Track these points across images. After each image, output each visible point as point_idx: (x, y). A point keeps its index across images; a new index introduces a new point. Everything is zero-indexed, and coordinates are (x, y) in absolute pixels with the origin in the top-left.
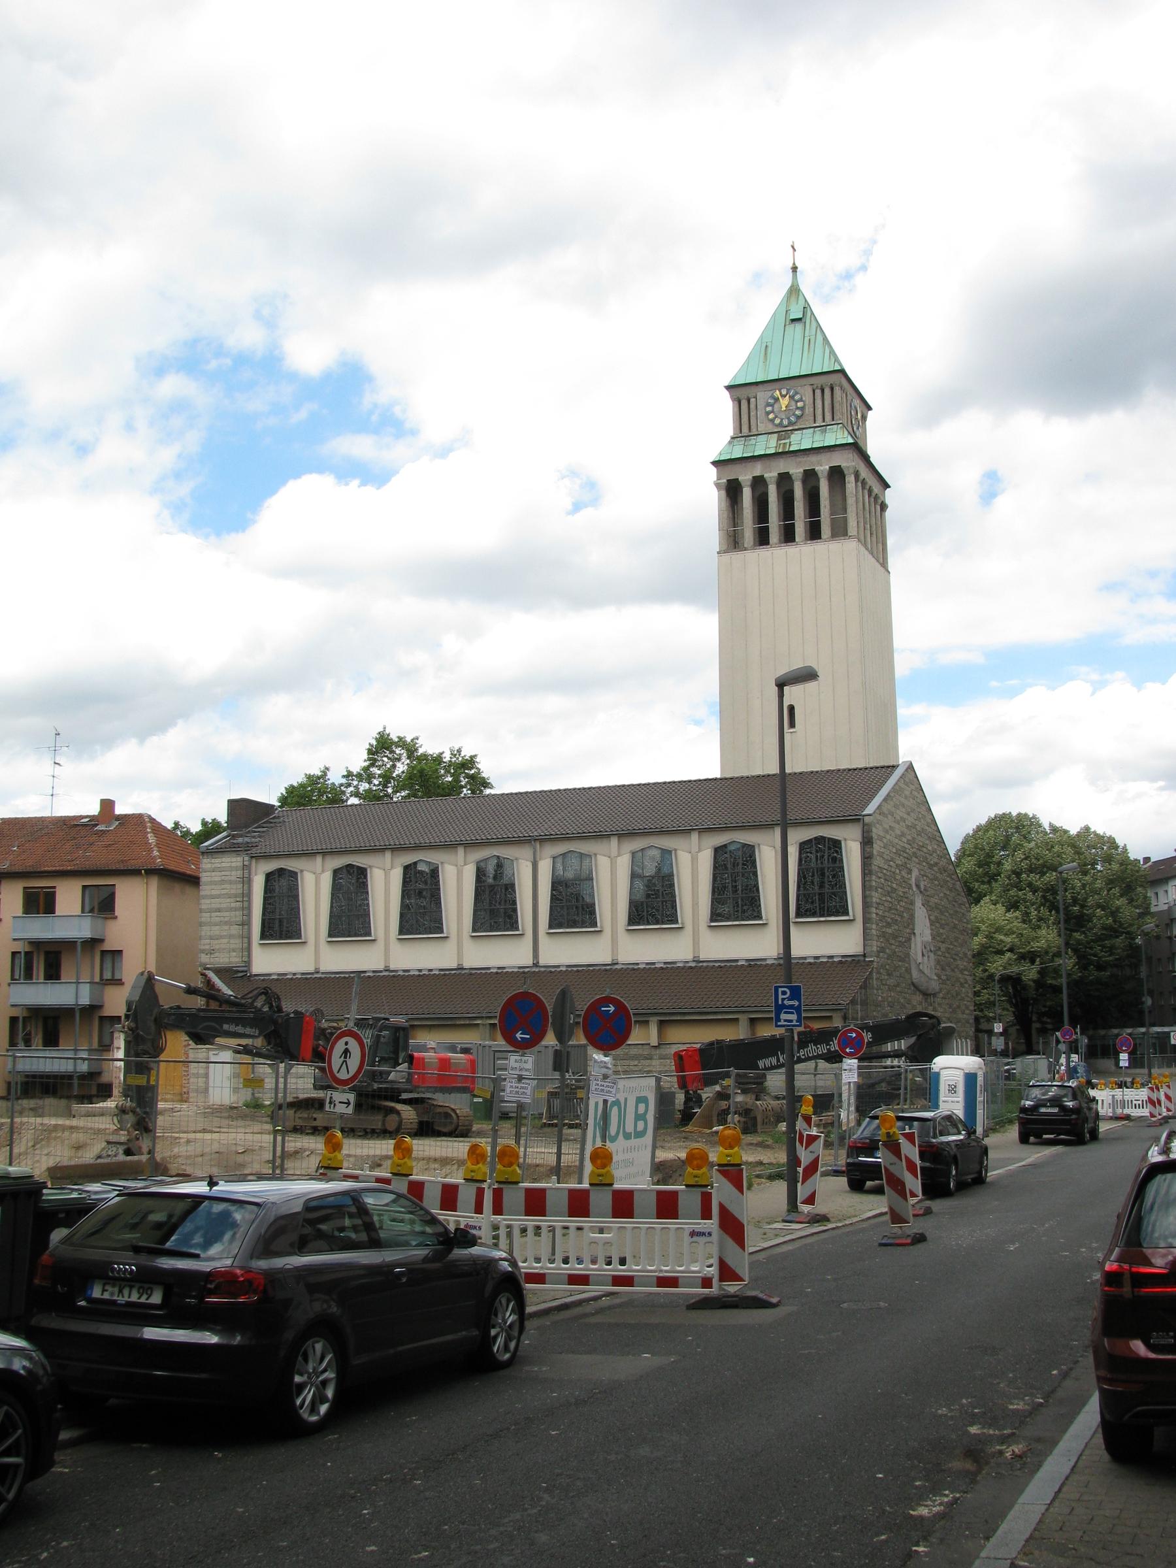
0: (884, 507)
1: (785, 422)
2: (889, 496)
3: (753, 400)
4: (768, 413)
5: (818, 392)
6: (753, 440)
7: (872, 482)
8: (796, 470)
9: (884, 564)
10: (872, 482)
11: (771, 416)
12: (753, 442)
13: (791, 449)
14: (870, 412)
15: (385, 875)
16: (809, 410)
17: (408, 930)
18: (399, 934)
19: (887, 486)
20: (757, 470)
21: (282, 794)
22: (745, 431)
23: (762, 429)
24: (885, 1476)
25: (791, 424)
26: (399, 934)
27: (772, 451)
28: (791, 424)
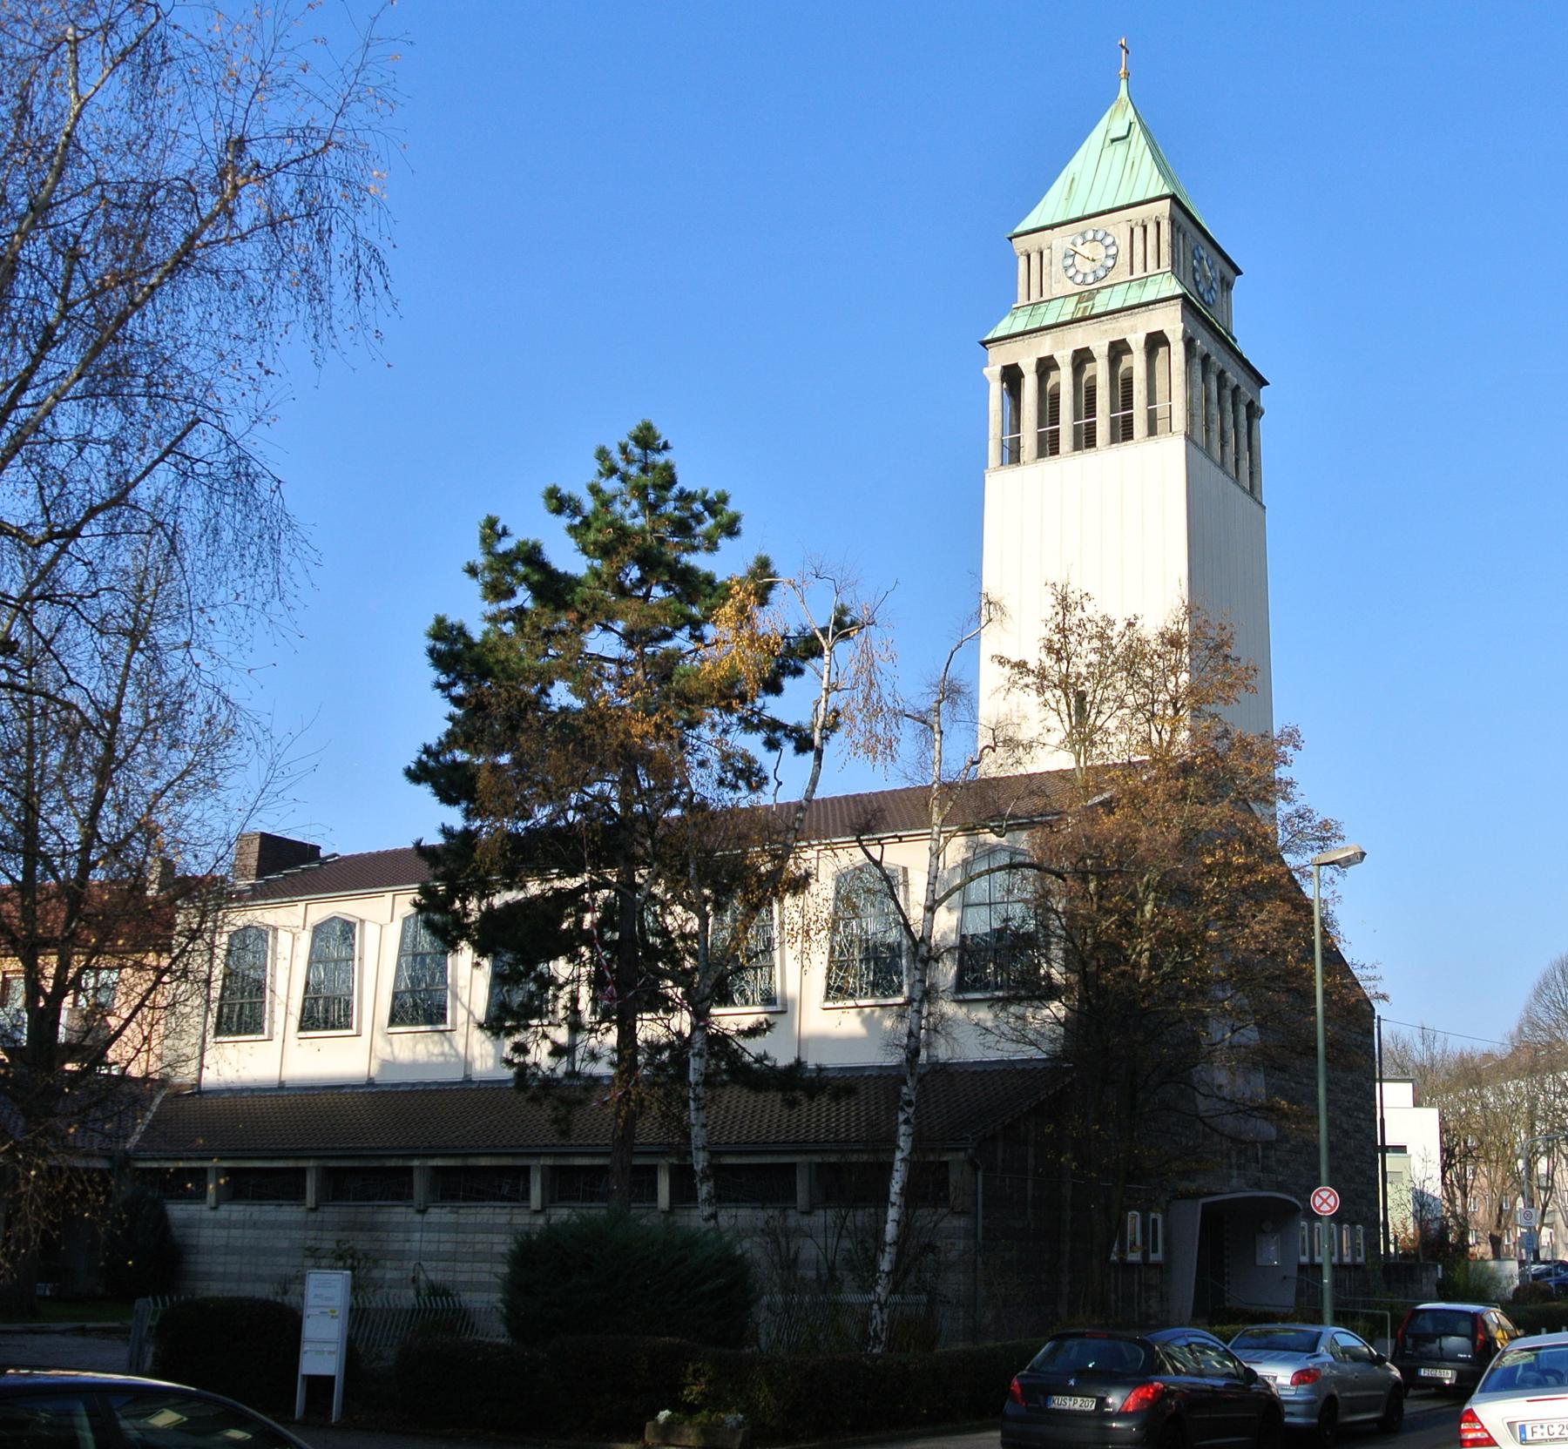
0: (1254, 411)
1: (1090, 279)
2: (1265, 397)
3: (1046, 252)
4: (1066, 269)
5: (1138, 232)
6: (1043, 308)
7: (1234, 376)
8: (1097, 340)
9: (1253, 491)
10: (1234, 376)
11: (1071, 272)
12: (1043, 309)
13: (1094, 312)
14: (1264, 389)
15: (972, 906)
16: (1124, 258)
17: (402, 1019)
18: (390, 1026)
19: (1262, 382)
20: (1044, 346)
21: (451, 718)
22: (1035, 297)
23: (1057, 292)
24: (1440, 1262)
25: (1097, 279)
26: (390, 1026)
27: (1068, 318)
28: (1097, 279)
